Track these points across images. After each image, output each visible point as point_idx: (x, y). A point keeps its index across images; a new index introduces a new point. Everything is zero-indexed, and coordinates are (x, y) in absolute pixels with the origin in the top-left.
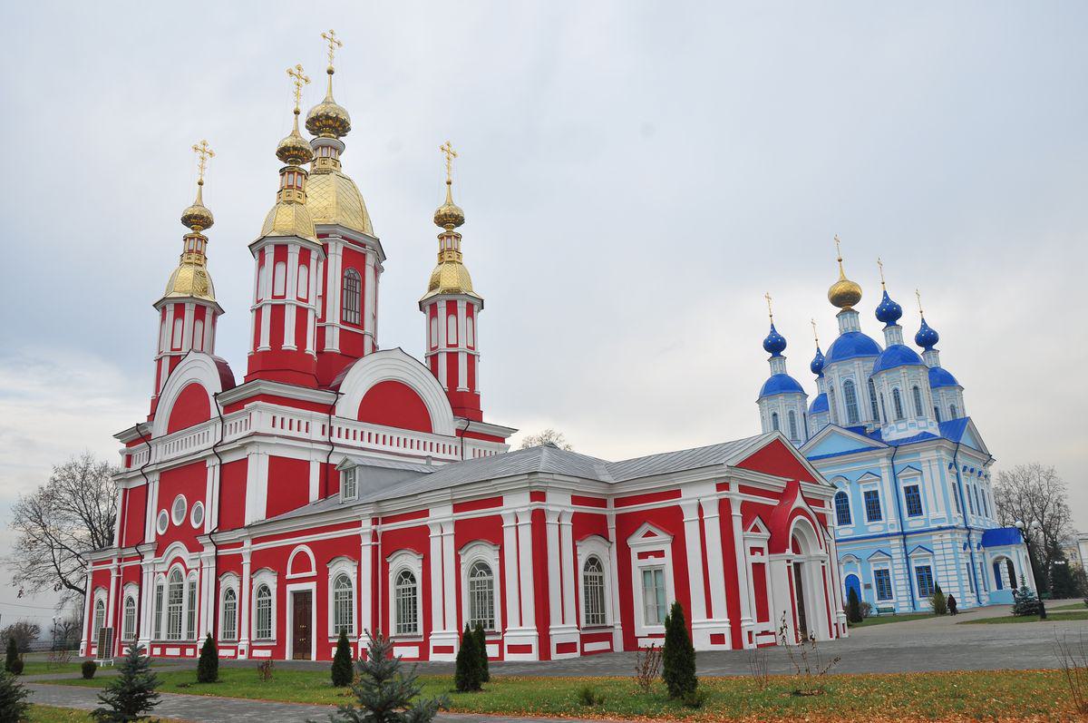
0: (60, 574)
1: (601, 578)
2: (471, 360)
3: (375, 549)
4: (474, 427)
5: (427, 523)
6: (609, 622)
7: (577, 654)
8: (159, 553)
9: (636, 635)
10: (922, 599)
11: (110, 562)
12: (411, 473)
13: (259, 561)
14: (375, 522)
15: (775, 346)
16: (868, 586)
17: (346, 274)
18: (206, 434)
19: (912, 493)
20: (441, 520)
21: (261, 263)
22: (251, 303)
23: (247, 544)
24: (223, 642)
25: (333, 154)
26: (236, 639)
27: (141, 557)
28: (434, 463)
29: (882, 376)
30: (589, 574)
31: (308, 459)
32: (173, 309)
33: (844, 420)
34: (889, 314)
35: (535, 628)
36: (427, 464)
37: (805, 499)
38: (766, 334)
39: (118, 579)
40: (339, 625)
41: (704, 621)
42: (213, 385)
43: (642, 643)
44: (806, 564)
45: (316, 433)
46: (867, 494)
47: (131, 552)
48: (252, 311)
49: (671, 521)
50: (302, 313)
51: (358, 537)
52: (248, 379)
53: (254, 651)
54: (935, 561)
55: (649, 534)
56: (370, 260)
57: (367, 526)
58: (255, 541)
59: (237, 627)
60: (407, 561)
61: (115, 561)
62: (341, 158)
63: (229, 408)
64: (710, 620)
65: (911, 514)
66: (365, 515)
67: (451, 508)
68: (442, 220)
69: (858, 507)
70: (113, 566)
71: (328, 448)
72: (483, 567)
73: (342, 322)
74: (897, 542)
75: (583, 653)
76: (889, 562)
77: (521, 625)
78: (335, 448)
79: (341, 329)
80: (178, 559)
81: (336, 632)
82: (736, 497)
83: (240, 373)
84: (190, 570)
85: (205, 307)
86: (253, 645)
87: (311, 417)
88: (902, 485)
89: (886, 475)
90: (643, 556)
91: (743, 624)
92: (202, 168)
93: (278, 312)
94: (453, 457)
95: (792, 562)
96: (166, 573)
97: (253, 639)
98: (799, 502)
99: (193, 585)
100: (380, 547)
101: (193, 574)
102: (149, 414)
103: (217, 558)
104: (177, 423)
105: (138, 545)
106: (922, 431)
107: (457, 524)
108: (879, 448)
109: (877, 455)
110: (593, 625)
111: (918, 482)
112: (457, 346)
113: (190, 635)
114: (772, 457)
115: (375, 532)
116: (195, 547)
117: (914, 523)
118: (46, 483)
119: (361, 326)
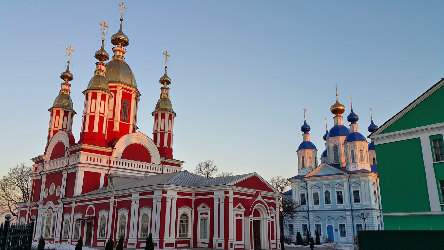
0: (10, 210)
1: (187, 221)
2: (169, 136)
3: (114, 207)
4: (168, 161)
5: (131, 199)
6: (189, 236)
8: (44, 205)
9: (197, 242)
10: (341, 237)
11: (27, 207)
13: (77, 210)
14: (115, 198)
15: (305, 129)
16: (336, 230)
17: (123, 102)
18: (63, 161)
19: (356, 194)
20: (136, 198)
22: (152, 131)
23: (74, 203)
24: (63, 239)
27: (38, 206)
28: (147, 174)
29: (347, 144)
30: (182, 219)
31: (100, 172)
33: (332, 161)
34: (353, 119)
35: (159, 238)
36: (145, 174)
38: (303, 124)
39: (29, 214)
40: (65, 235)
42: (67, 144)
43: (199, 245)
44: (262, 221)
45: (104, 163)
46: (338, 193)
47: (34, 204)
49: (210, 203)
50: (101, 119)
51: (109, 203)
52: (80, 142)
53: (73, 242)
54: (347, 222)
55: (204, 207)
56: (134, 96)
57: (112, 199)
58: (76, 202)
59: (68, 234)
60: (123, 212)
61: (28, 207)
62: (125, 56)
63: (73, 152)
64: (169, 237)
65: (355, 202)
66: (112, 195)
67: (139, 194)
69: (334, 198)
70: (27, 209)
71: (109, 168)
72: (145, 215)
73: (121, 120)
74: (349, 213)
76: (345, 221)
78: (111, 168)
79: (120, 123)
80: (51, 208)
81: (119, 237)
82: (231, 196)
83: (77, 139)
84: (54, 212)
85: (68, 112)
87: (102, 157)
88: (352, 190)
89: (346, 185)
90: (201, 214)
91: (229, 240)
92: (166, 61)
93: (92, 118)
94: (159, 172)
95: (253, 220)
96: (46, 212)
97: (73, 238)
98: (259, 198)
99: (55, 217)
101: (55, 213)
102: (45, 152)
103: (64, 208)
104: (54, 156)
105: (37, 201)
106: (362, 168)
108: (344, 174)
109: (342, 177)
110: (182, 238)
111: (342, 190)
113: (53, 236)
115: (115, 201)
116: (56, 203)
117: (356, 206)
118: (6, 174)
119: (129, 122)
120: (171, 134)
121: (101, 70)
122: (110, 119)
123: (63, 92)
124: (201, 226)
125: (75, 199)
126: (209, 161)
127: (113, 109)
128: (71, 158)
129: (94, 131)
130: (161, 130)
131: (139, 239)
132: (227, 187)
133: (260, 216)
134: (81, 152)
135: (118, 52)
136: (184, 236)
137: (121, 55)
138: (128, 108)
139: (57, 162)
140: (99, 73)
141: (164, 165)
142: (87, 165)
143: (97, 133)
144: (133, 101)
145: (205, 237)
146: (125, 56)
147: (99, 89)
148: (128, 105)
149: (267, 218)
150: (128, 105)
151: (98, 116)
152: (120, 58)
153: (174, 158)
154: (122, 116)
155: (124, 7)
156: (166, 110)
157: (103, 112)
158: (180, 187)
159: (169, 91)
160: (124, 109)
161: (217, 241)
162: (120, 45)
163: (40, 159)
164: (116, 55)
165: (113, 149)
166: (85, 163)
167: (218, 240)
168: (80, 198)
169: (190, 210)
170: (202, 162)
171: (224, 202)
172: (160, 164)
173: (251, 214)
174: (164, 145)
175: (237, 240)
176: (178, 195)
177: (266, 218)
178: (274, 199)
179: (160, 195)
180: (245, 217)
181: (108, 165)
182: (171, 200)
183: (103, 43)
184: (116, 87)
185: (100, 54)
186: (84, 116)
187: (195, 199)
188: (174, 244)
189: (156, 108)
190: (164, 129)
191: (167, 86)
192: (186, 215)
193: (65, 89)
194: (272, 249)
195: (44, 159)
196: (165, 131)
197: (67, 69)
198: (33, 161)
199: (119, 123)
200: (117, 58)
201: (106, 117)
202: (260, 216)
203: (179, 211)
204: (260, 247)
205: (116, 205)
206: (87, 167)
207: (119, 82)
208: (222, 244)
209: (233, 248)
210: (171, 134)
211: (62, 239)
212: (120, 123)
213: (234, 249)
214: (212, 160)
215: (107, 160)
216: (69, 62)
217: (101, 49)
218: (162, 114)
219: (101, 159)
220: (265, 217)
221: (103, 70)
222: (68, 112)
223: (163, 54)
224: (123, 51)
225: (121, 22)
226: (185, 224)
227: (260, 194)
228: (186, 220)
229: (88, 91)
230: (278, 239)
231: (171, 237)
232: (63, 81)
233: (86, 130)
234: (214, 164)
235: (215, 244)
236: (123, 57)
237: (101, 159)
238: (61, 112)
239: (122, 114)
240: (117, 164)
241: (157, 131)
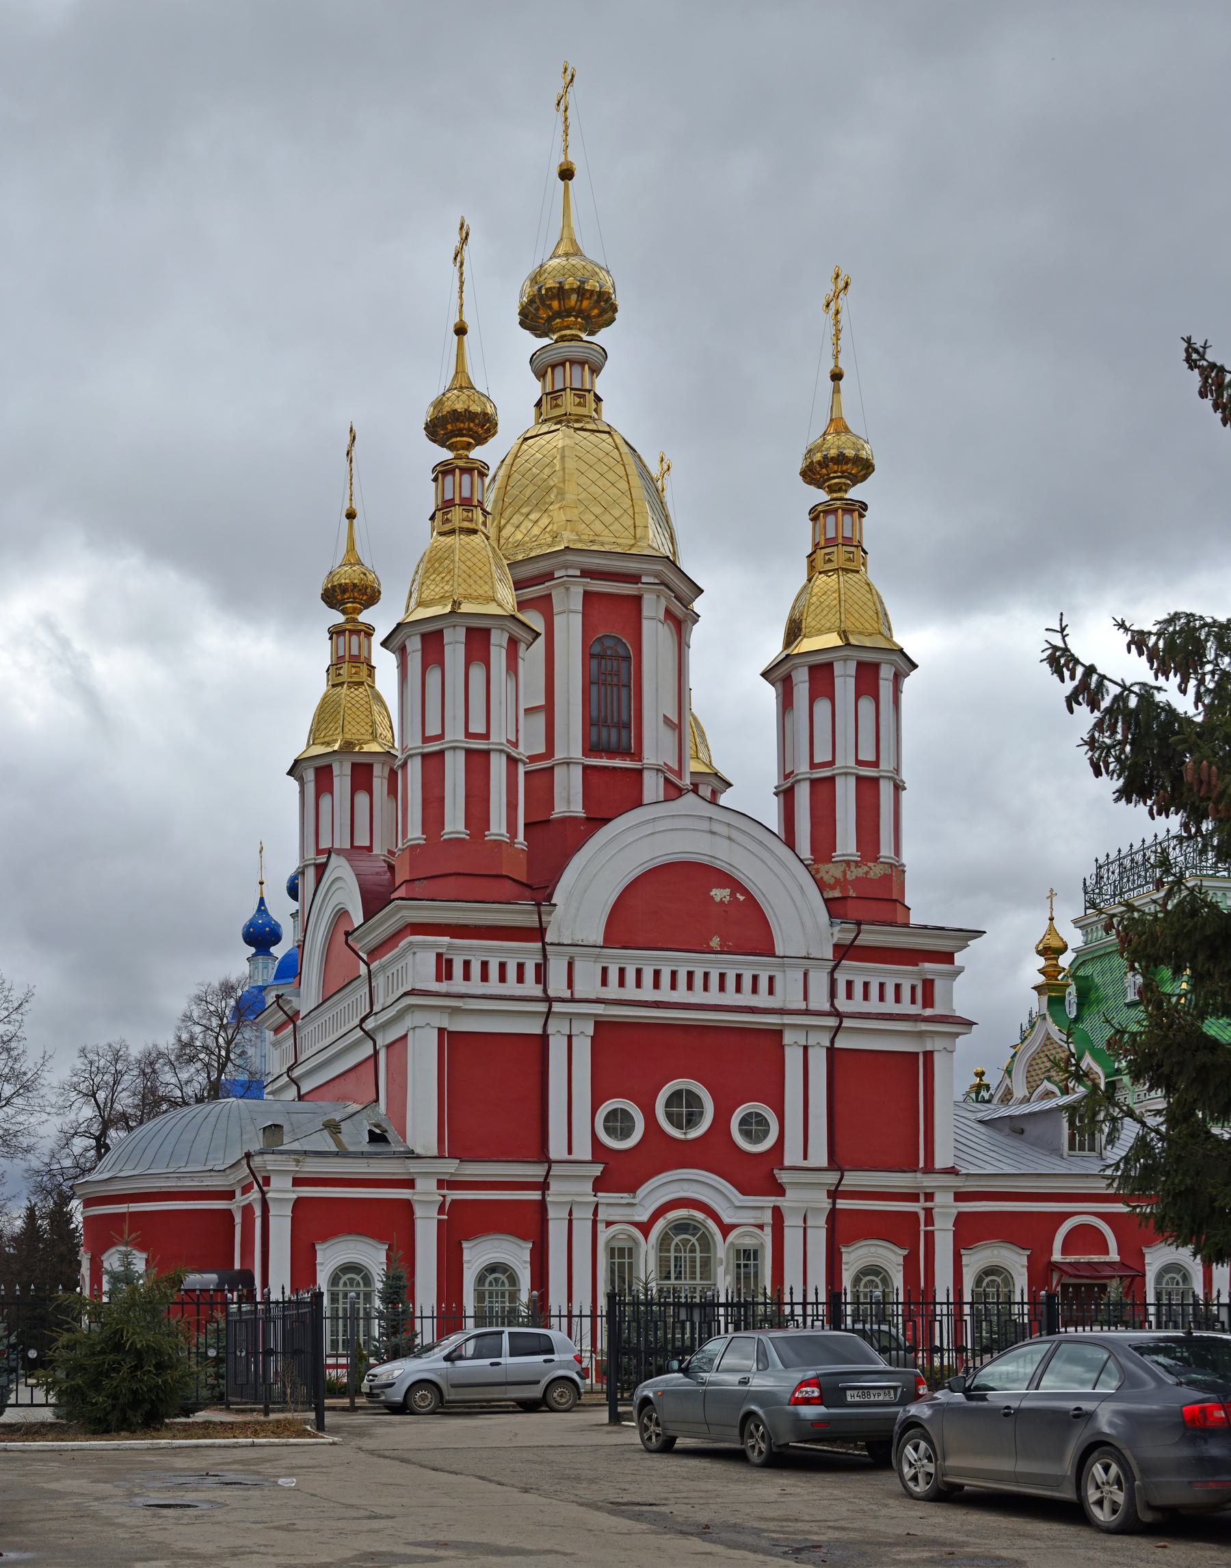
2: (867, 787)
21: (786, 702)
22: (772, 779)
25: (577, 376)
32: (419, 646)
48: (776, 794)
50: (477, 761)
56: (653, 608)
62: (602, 384)
71: (832, 1022)
93: (823, 788)
100: (327, 1349)
107: (500, 1356)
114: (232, 987)
122: (533, 759)
127: (542, 702)
137: (577, 385)
144: (655, 635)
146: (602, 384)
153: (914, 919)
159: (864, 520)
163: (285, 1012)
164: (547, 394)
174: (448, 828)
176: (956, 1200)
186: (781, 789)
190: (873, 759)
219: (771, 979)
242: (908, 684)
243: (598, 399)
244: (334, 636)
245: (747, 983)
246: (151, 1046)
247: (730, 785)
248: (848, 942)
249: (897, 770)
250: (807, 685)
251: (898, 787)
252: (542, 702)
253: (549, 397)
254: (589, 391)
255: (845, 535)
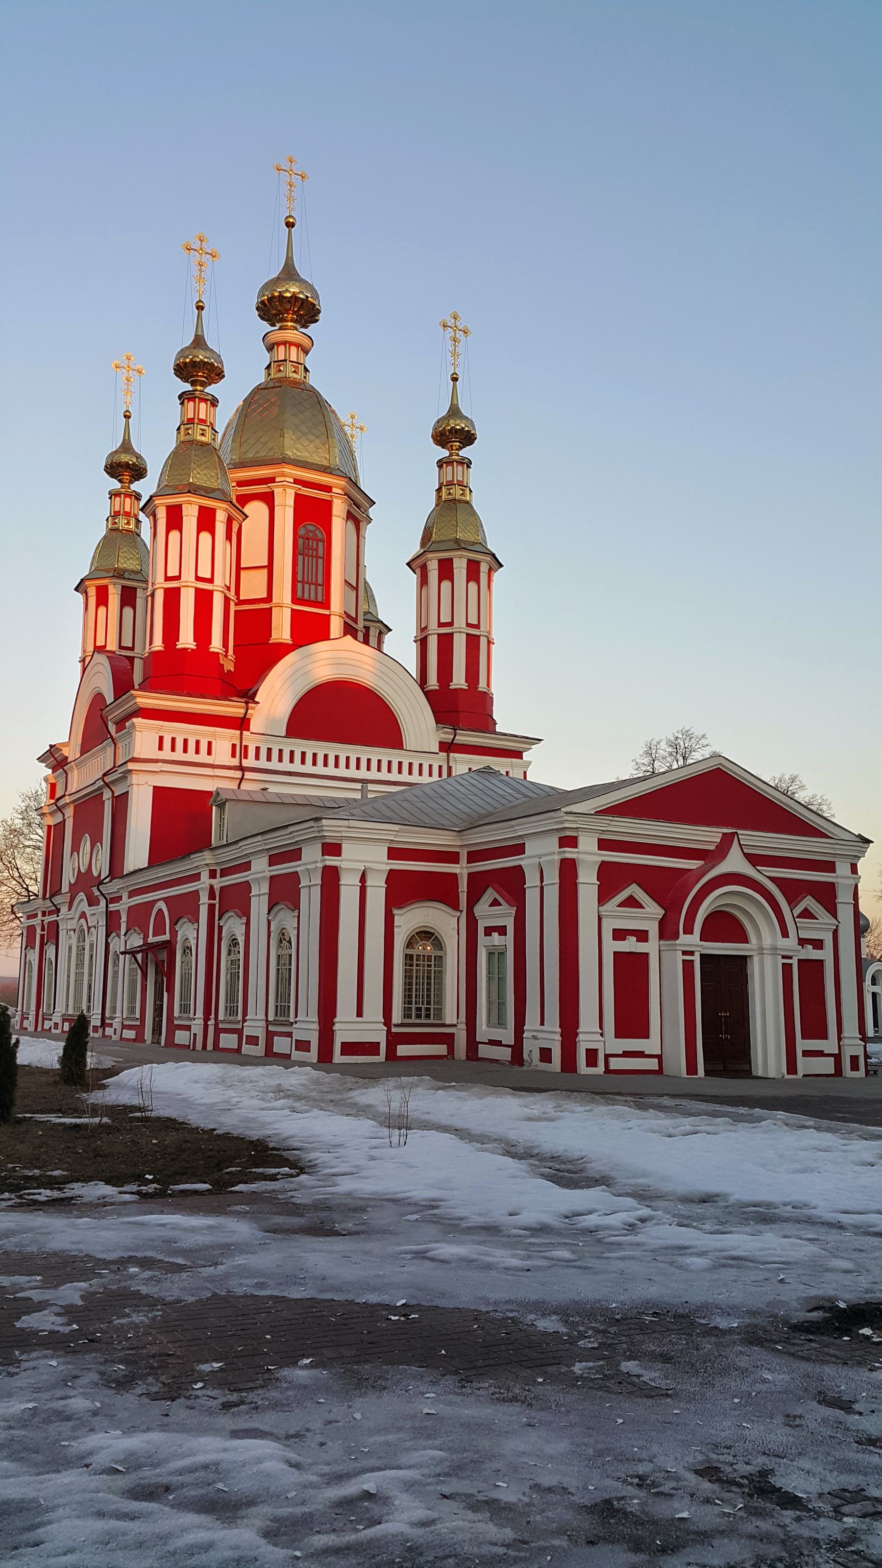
2: (473, 642)
6: (450, 1016)
7: (382, 1057)
12: (308, 807)
14: (213, 874)
17: (302, 532)
21: (424, 581)
26: (240, 1017)
27: (58, 911)
28: (371, 787)
37: (749, 857)
40: (279, 1004)
41: (537, 1028)
43: (484, 1051)
45: (222, 754)
48: (415, 641)
50: (203, 600)
51: (196, 893)
55: (495, 903)
56: (339, 508)
58: (132, 894)
60: (233, 926)
62: (309, 361)
64: (359, 1019)
68: (442, 437)
71: (238, 774)
73: (295, 600)
75: (607, 1070)
77: (542, 1024)
79: (292, 610)
86: (221, 1026)
87: (214, 735)
90: (489, 931)
91: (581, 1037)
92: (454, 354)
93: (446, 642)
96: (74, 930)
99: (92, 945)
110: (418, 1021)
112: (451, 624)
115: (212, 887)
120: (478, 637)
121: (196, 421)
123: (116, 521)
124: (489, 979)
125: (125, 883)
126: (688, 734)
127: (266, 564)
128: (119, 745)
129: (179, 646)
130: (439, 626)
131: (222, 1022)
132: (562, 822)
133: (745, 939)
134: (135, 720)
135: (282, 348)
136: (428, 1016)
137: (293, 358)
138: (321, 553)
139: (93, 762)
140: (190, 432)
141: (451, 755)
142: (160, 764)
143: (192, 650)
144: (339, 525)
145: (501, 1023)
146: (309, 361)
147: (193, 490)
148: (320, 544)
149: (777, 949)
150: (320, 544)
151: (189, 588)
152: (288, 371)
154: (300, 585)
155: (296, 174)
156: (459, 545)
157: (208, 576)
158: (397, 827)
159: (470, 470)
160: (306, 558)
161: (535, 1037)
162: (287, 321)
163: (55, 759)
164: (275, 362)
165: (247, 703)
166: (155, 757)
167: (539, 1035)
168: (134, 880)
169: (454, 916)
170: (657, 739)
171: (557, 881)
172: (438, 751)
173: (689, 930)
174: (455, 680)
175: (620, 1033)
177: (775, 948)
178: (829, 867)
179: (317, 862)
180: (661, 942)
181: (238, 764)
182: (363, 879)
183: (199, 317)
184: (272, 480)
185: (188, 360)
186: (418, 638)
187: (469, 874)
188: (378, 1043)
189: (423, 545)
190: (450, 620)
191: (462, 453)
192: (433, 934)
193: (119, 512)
194: (804, 1076)
195: (67, 755)
196: (455, 625)
197: (124, 440)
198: (44, 764)
199: (289, 610)
200: (280, 370)
201: (486, 636)
202: (745, 939)
203: (397, 921)
204: (748, 1069)
205: (215, 899)
206: (161, 771)
207: (285, 461)
208: (550, 1049)
209: (600, 1069)
210: (478, 637)
211: (176, 1018)
212: (292, 610)
213: (602, 1073)
214: (697, 732)
215: (234, 746)
216: (128, 414)
217: (194, 341)
218: (440, 561)
219: (210, 744)
220: (767, 942)
221: (204, 418)
222: (135, 589)
223: (441, 328)
224: (297, 341)
225: (290, 232)
226: (429, 972)
227: (740, 845)
228: (496, 954)
229: (154, 501)
230: (845, 1034)
231: (367, 1015)
232: (115, 485)
233: (430, 684)
234: (707, 745)
235: (530, 1048)
236: (301, 364)
237: (210, 744)
238: (110, 592)
239: (300, 578)
240: (185, 750)
241: (426, 628)
242: (496, 576)
243: (306, 370)
244: (113, 497)
245: (363, 764)
246: (664, 749)
247: (390, 630)
248: (450, 741)
249: (489, 632)
250: (437, 572)
251: (489, 643)
252: (266, 564)
253: (276, 364)
254: (301, 364)
255: (200, 417)
